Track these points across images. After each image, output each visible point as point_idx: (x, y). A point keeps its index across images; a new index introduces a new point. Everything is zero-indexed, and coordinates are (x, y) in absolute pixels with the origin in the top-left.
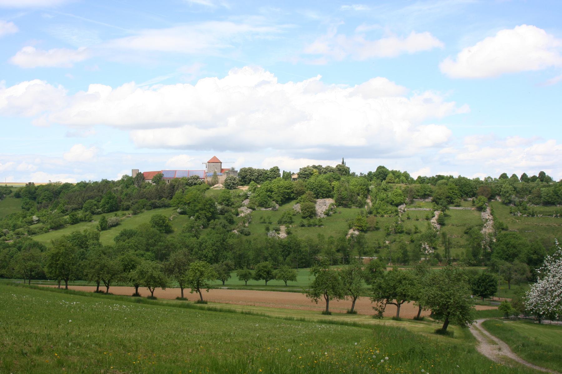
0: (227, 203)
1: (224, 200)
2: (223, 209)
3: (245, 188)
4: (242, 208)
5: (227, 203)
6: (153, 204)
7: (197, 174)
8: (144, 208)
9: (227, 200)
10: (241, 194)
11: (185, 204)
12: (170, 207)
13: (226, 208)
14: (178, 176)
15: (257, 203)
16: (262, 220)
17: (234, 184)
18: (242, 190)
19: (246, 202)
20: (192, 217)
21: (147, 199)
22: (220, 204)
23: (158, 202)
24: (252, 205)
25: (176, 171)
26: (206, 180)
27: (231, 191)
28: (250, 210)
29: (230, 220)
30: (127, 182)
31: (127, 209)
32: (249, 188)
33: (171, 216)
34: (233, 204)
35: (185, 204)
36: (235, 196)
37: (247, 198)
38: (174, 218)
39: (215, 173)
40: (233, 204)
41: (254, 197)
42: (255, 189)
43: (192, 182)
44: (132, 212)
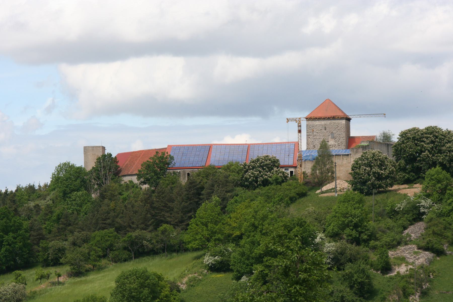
0: (354, 233)
1: (344, 226)
2: (342, 253)
3: (413, 191)
4: (402, 248)
5: (354, 233)
6: (133, 243)
7: (272, 154)
8: (104, 256)
9: (356, 226)
10: (401, 206)
11: (228, 238)
12: (186, 250)
13: (353, 248)
14: (216, 159)
17: (379, 177)
18: (405, 195)
19: (415, 231)
20: (244, 279)
21: (118, 230)
22: (335, 236)
23: (149, 235)
24: (434, 240)
25: (210, 147)
26: (299, 171)
27: (370, 200)
28: (428, 255)
29: (362, 284)
30: (69, 180)
31: (56, 263)
32: (425, 190)
33: (182, 276)
34: (373, 236)
35: (228, 238)
36: (380, 214)
38: (192, 284)
39: (324, 146)
40: (373, 236)
41: (440, 215)
42: (443, 191)
43: (258, 175)
44: (68, 268)
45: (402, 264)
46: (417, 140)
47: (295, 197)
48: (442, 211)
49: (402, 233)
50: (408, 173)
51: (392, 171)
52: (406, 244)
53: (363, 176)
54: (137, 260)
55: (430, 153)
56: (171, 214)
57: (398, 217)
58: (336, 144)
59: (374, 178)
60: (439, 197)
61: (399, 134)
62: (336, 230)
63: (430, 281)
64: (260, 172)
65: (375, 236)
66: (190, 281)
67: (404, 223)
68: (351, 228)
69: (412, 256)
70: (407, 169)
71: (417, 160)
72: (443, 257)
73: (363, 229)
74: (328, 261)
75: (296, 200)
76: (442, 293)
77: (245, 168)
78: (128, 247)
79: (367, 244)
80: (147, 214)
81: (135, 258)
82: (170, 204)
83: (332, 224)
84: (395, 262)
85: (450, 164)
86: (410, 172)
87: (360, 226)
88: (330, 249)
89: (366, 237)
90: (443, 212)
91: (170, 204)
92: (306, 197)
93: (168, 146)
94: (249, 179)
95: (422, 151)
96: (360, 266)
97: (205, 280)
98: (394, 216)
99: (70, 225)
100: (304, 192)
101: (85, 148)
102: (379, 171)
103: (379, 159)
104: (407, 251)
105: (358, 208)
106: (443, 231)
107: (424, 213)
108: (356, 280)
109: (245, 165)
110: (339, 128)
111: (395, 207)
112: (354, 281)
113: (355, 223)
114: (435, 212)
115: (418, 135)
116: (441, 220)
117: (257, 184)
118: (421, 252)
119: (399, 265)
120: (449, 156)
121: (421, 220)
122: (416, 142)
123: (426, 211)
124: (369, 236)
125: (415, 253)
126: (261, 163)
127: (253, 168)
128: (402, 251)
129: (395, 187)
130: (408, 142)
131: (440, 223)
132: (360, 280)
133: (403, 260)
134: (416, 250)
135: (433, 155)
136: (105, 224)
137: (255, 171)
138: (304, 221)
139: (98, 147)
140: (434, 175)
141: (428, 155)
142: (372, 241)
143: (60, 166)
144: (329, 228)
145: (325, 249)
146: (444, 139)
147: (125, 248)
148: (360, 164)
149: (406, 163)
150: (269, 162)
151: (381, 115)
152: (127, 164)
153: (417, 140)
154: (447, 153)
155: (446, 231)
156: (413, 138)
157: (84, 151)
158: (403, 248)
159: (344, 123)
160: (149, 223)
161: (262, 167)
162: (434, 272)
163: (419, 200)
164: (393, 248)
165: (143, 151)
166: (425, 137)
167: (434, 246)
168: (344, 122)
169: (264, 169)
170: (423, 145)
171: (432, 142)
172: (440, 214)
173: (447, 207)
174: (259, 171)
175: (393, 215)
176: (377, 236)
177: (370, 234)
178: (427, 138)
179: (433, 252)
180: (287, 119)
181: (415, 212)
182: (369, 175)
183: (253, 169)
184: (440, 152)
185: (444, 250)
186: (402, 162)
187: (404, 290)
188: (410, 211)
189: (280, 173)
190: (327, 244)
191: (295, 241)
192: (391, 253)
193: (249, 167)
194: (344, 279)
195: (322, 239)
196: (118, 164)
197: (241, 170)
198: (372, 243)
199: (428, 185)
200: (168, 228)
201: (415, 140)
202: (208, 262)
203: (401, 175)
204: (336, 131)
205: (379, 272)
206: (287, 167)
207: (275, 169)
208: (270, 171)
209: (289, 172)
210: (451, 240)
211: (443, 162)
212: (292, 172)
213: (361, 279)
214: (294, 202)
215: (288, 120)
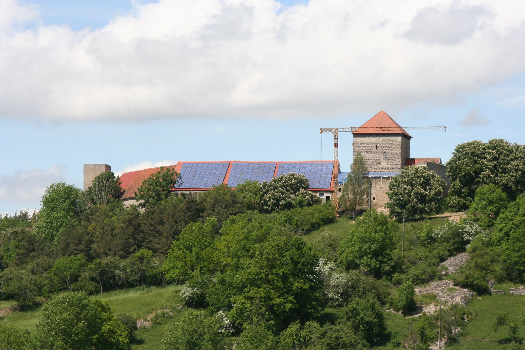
1: (362, 254)
4: (434, 284)
14: (233, 182)
15: (498, 268)
16: (504, 332)
17: (423, 199)
19: (453, 264)
23: (123, 263)
34: (397, 267)
37: (460, 247)
41: (489, 244)
45: (431, 303)
46: (477, 156)
47: (318, 223)
48: (490, 239)
49: (438, 265)
50: (464, 198)
51: (439, 191)
52: (440, 279)
53: (403, 197)
54: (105, 294)
55: (493, 173)
56: (160, 240)
57: (436, 245)
58: (390, 166)
59: (415, 200)
60: (490, 222)
61: (455, 148)
62: (351, 258)
63: (463, 325)
64: (283, 193)
65: (401, 268)
66: (157, 317)
67: (441, 253)
68: (369, 256)
69: (445, 293)
70: (463, 193)
71: (474, 181)
72: (487, 297)
73: (384, 258)
74: (336, 297)
75: (319, 226)
76: (476, 340)
77: (265, 189)
78: (96, 278)
79: (389, 278)
80: (129, 238)
81: (104, 291)
82: (159, 228)
83: (347, 251)
84: (423, 300)
85: (517, 187)
86: (466, 196)
87: (381, 255)
88: (339, 281)
89: (388, 268)
90: (492, 240)
91: (159, 228)
92: (332, 224)
93: (179, 162)
94: (269, 201)
95: (481, 170)
96: (368, 301)
97: (177, 317)
98: (431, 245)
99: (34, 250)
100: (331, 217)
101: (85, 165)
102: (422, 191)
103: (424, 177)
104: (440, 287)
105: (381, 231)
106: (489, 263)
107: (468, 242)
108: (362, 319)
109: (265, 184)
110: (393, 147)
111: (432, 234)
112: (359, 321)
113: (374, 250)
114: (482, 240)
115: (479, 149)
116: (488, 250)
117: (278, 208)
118: (457, 290)
119: (427, 304)
120: (516, 177)
121: (464, 250)
122: (476, 158)
123: (471, 238)
124: (392, 267)
125: (450, 290)
126: (285, 182)
127: (275, 188)
128: (435, 287)
129: (446, 214)
130: (465, 158)
131: (487, 254)
132: (367, 319)
133: (433, 298)
134: (451, 286)
135: (497, 176)
136: (77, 250)
137: (276, 192)
138: (302, 243)
139: (99, 165)
140: (485, 194)
141: (489, 175)
142: (397, 274)
143: (52, 187)
144: (342, 256)
145: (332, 281)
146: (508, 155)
147: (93, 279)
148: (399, 181)
149: (462, 184)
150: (294, 181)
151: (441, 128)
152: (131, 185)
153: (477, 156)
154: (513, 172)
155: (493, 264)
156: (472, 153)
157: (84, 170)
158: (435, 284)
159: (401, 140)
160: (131, 250)
161: (286, 187)
162: (471, 314)
163: (464, 225)
164: (422, 283)
165: (151, 169)
166: (487, 152)
167: (475, 282)
168: (399, 139)
169: (287, 190)
170: (483, 163)
171: (495, 159)
172: (488, 243)
173: (498, 234)
174: (281, 192)
175: (429, 243)
176: (403, 267)
177: (393, 264)
178: (489, 153)
179: (473, 290)
180: (321, 129)
181: (456, 239)
182: (410, 196)
183: (274, 190)
184: (504, 171)
185: (487, 287)
186: (457, 182)
187: (422, 332)
188: (450, 238)
189: (308, 195)
190: (336, 275)
191: (264, 257)
192: (417, 290)
193: (269, 186)
194: (348, 318)
195: (332, 269)
196: (121, 186)
197: (259, 190)
198: (396, 276)
199: (477, 207)
200: (145, 254)
201: (474, 156)
202: (185, 295)
203: (455, 199)
204: (389, 151)
205: (400, 313)
206: (322, 192)
207: (302, 190)
208: (295, 193)
209: (324, 197)
210: (498, 276)
211: (507, 184)
212: (328, 198)
213: (368, 318)
214: (317, 229)
215: (322, 131)
